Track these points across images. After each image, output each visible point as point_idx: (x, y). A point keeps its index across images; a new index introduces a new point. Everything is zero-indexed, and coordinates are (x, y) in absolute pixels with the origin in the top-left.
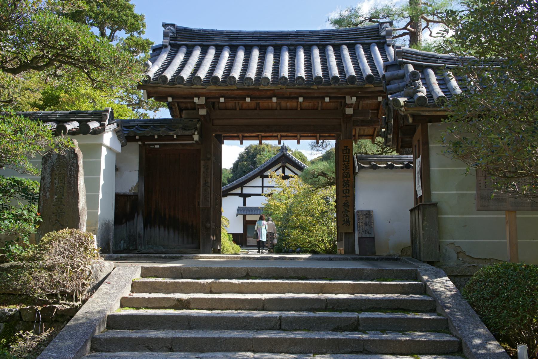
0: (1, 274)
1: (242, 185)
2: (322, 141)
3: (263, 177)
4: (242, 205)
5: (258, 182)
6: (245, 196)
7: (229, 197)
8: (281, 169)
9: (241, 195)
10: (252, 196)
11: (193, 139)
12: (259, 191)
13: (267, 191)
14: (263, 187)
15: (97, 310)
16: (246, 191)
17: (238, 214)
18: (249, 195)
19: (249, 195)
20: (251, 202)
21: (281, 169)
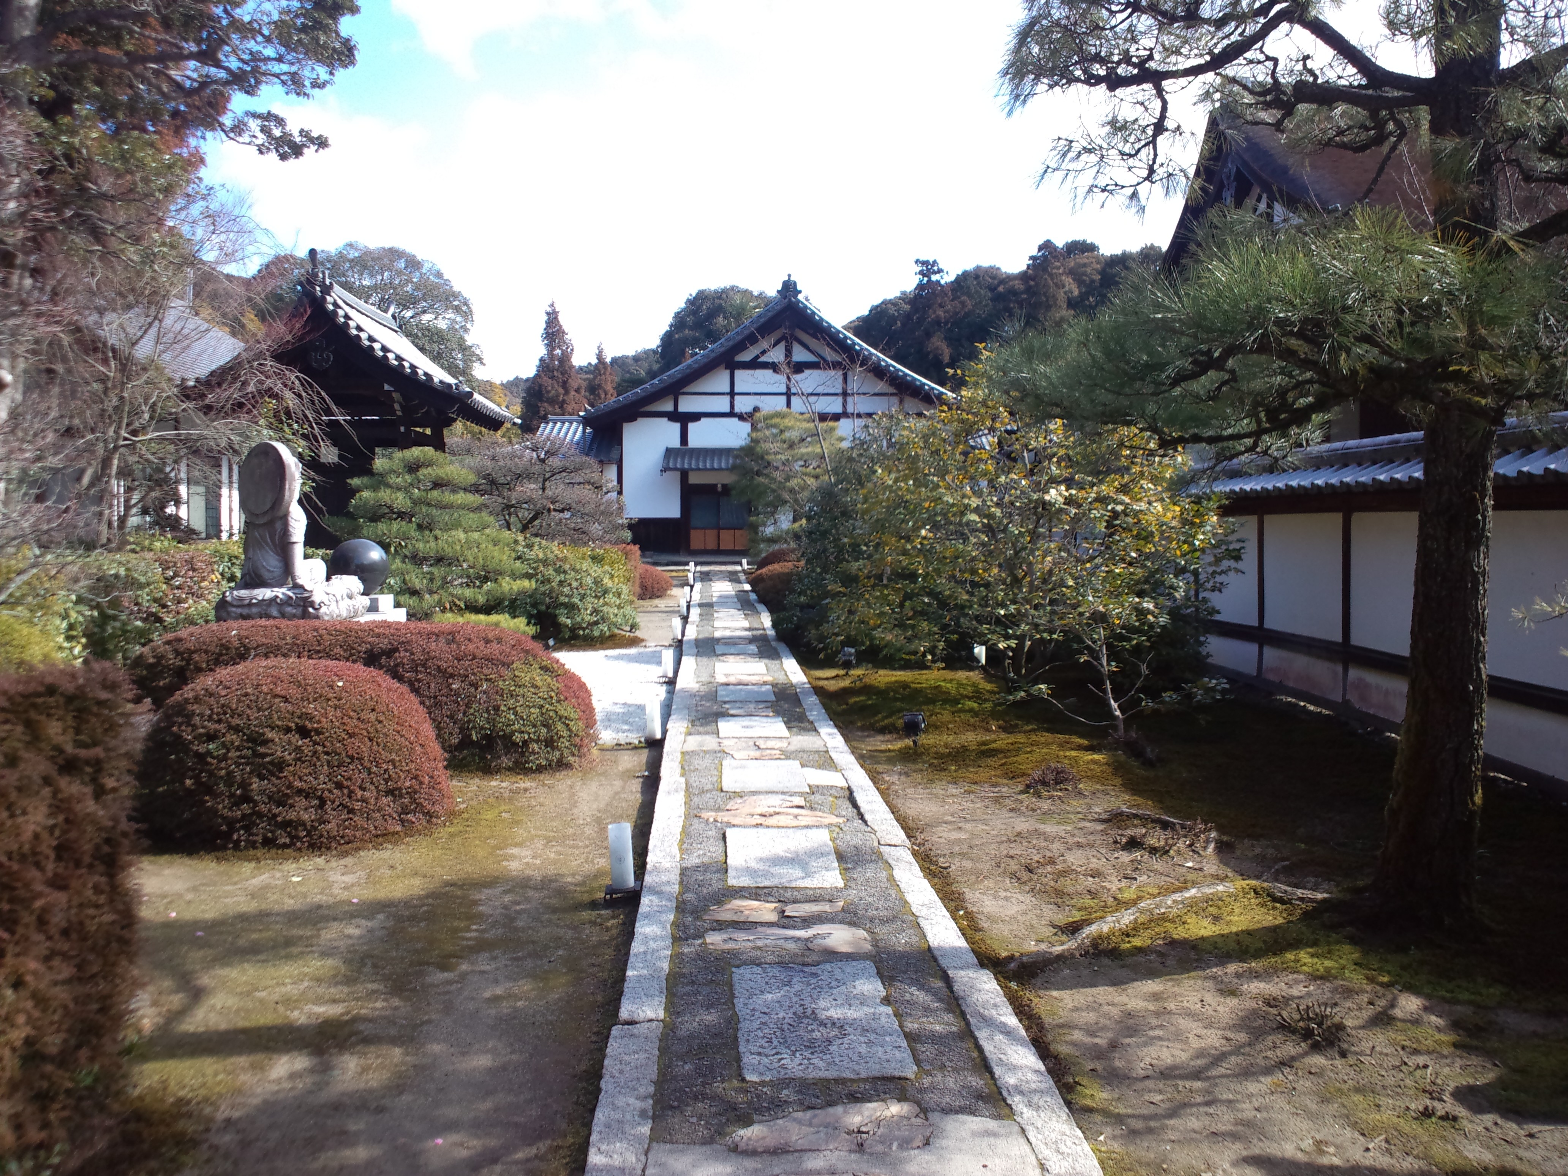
0: (5, 283)
1: (675, 389)
2: (382, 987)
3: (733, 366)
4: (676, 443)
5: (720, 381)
6: (685, 419)
7: (642, 422)
8: (782, 345)
9: (675, 416)
10: (703, 420)
11: (394, 414)
12: (722, 404)
13: (743, 405)
14: (732, 394)
15: (396, 684)
16: (687, 405)
17: (665, 469)
18: (696, 417)
19: (696, 417)
20: (703, 435)
21: (782, 345)
